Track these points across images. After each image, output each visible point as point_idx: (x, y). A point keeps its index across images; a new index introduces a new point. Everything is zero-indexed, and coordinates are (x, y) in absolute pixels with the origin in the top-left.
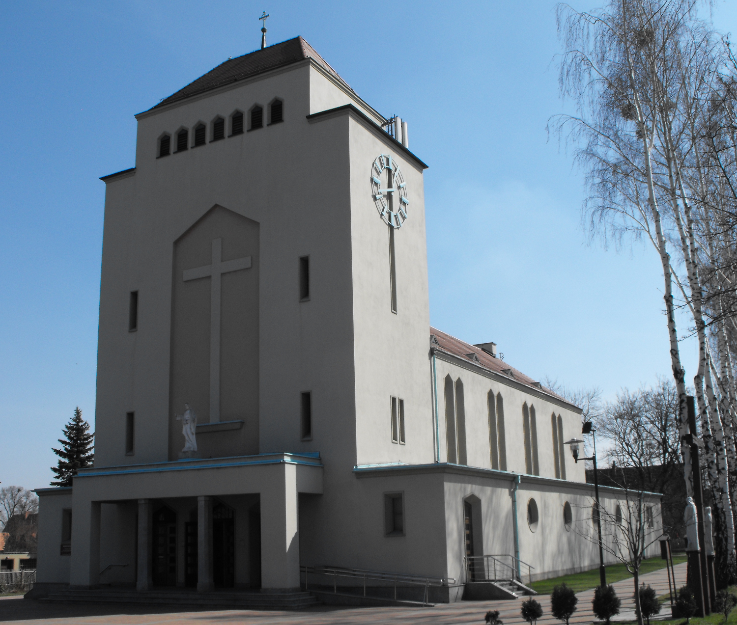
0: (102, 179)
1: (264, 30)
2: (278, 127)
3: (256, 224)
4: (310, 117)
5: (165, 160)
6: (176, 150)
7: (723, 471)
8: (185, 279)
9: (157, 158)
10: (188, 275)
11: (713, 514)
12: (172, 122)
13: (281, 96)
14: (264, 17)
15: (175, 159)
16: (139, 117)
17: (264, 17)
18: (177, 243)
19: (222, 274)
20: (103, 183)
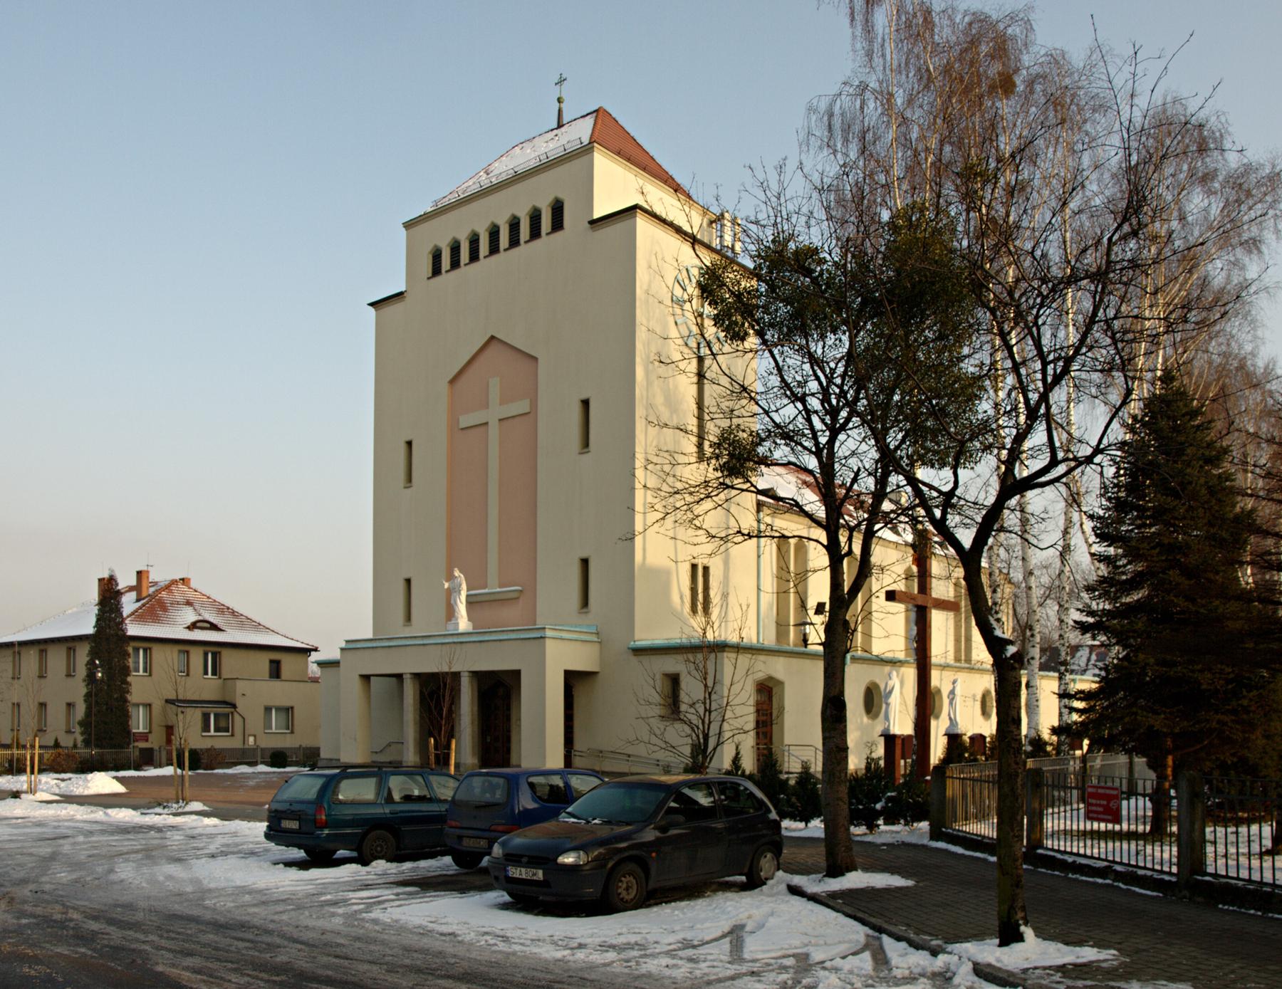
0: (372, 304)
1: (560, 100)
2: (558, 235)
3: (535, 359)
4: (593, 222)
5: (438, 279)
6: (550, 230)
7: (1032, 662)
8: (463, 425)
9: (429, 278)
10: (465, 421)
11: (979, 567)
12: (459, 228)
13: (561, 196)
14: (561, 81)
15: (448, 279)
16: (408, 225)
17: (561, 81)
18: (453, 381)
19: (150, 705)
20: (372, 309)
